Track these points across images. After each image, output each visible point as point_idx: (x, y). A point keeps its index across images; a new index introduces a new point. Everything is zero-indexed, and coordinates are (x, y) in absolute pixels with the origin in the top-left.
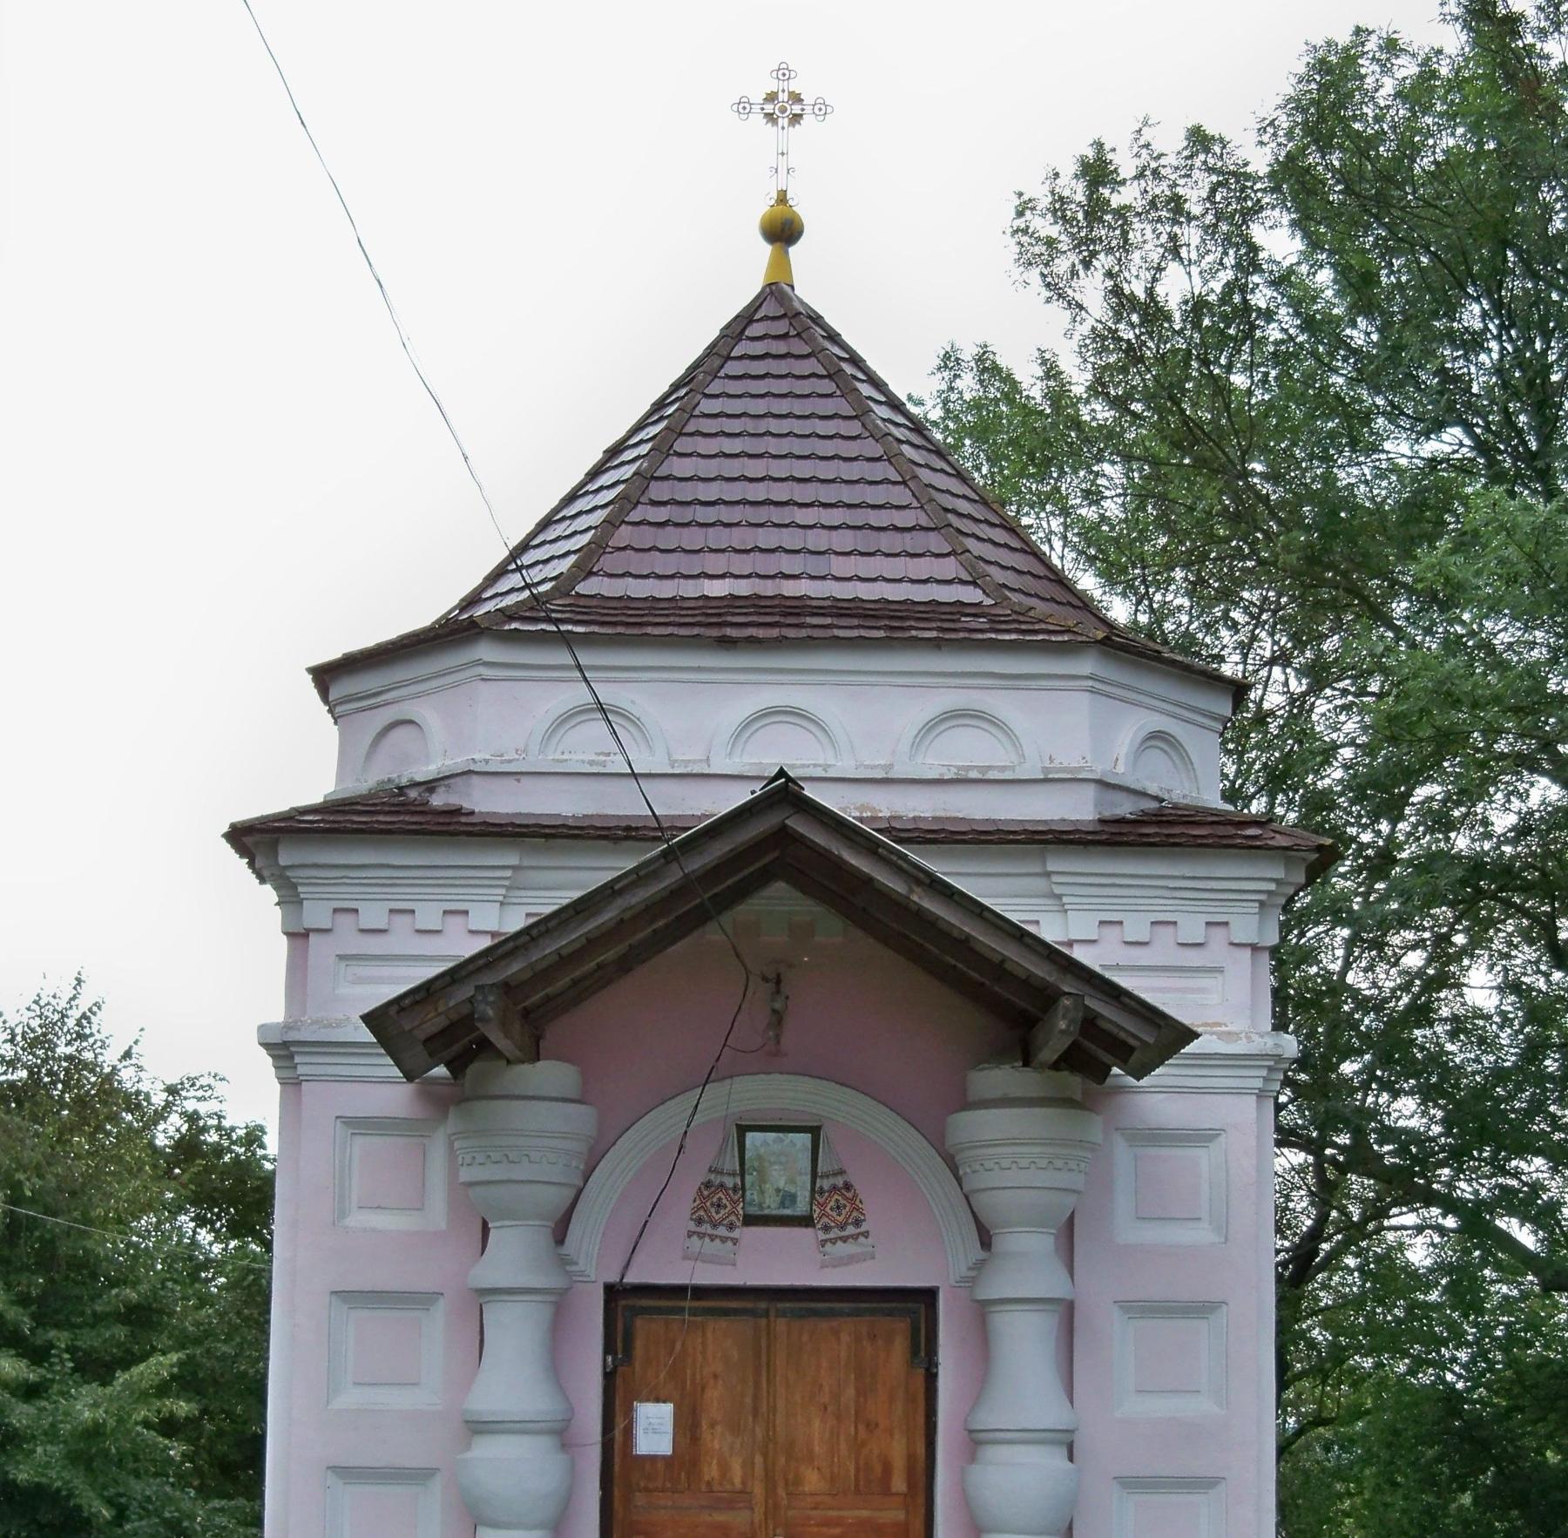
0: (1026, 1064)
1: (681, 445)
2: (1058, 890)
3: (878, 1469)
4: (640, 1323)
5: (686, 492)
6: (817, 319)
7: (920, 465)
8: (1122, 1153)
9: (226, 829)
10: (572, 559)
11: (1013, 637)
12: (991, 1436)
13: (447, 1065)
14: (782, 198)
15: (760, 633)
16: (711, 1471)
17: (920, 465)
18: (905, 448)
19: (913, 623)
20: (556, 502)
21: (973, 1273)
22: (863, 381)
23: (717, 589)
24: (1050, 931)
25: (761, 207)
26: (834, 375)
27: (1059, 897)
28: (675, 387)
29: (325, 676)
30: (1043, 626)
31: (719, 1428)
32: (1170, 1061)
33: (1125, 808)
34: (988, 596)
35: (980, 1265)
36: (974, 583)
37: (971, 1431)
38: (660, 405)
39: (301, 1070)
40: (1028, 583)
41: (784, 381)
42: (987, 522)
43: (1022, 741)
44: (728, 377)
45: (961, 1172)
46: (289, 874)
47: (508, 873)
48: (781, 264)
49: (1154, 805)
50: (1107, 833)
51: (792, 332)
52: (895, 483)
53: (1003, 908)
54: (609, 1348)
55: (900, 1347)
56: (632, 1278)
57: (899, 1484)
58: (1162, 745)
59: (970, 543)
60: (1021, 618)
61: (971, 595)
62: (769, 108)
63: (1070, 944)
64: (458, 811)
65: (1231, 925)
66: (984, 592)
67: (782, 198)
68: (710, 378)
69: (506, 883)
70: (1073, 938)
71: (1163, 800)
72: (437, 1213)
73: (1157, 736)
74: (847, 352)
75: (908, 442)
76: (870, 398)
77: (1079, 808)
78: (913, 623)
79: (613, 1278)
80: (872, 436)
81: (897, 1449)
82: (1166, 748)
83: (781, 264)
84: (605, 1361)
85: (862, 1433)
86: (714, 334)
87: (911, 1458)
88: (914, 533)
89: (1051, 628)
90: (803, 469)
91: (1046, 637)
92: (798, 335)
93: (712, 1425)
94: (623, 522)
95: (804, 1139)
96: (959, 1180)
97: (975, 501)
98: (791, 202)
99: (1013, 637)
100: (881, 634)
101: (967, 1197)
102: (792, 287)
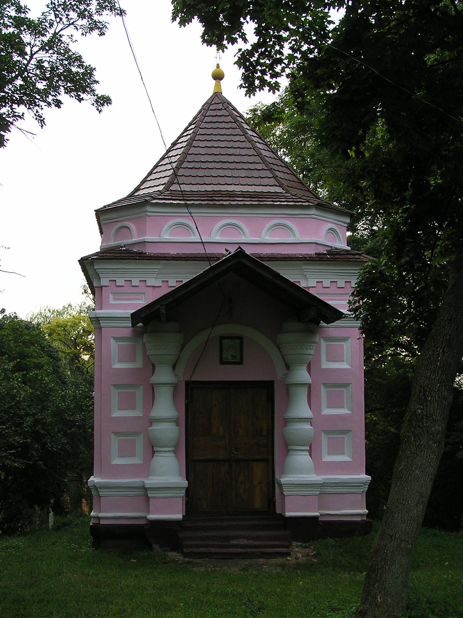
0: (299, 321)
1: (195, 144)
2: (305, 273)
5: (197, 158)
6: (230, 104)
7: (262, 149)
8: (323, 345)
9: (80, 259)
10: (167, 179)
11: (292, 203)
12: (291, 420)
13: (142, 323)
15: (225, 203)
17: (262, 149)
18: (263, 152)
19: (265, 199)
20: (159, 159)
21: (285, 377)
22: (244, 123)
23: (209, 188)
24: (303, 285)
25: (212, 68)
26: (236, 121)
27: (306, 275)
28: (190, 124)
29: (99, 213)
30: (300, 200)
32: (337, 322)
33: (323, 250)
34: (284, 190)
35: (286, 374)
36: (280, 186)
37: (284, 419)
38: (186, 130)
39: (101, 324)
40: (295, 185)
41: (215, 118)
42: (281, 166)
43: (295, 232)
44: (206, 122)
45: (281, 350)
46: (97, 271)
48: (218, 86)
49: (330, 248)
50: (319, 258)
51: (223, 108)
52: (256, 156)
53: (326, 298)
54: (186, 398)
58: (331, 231)
59: (277, 173)
60: (294, 197)
61: (279, 190)
63: (308, 288)
64: (142, 253)
65: (352, 282)
66: (283, 189)
68: (201, 123)
69: (157, 273)
70: (309, 286)
71: (332, 247)
72: (138, 364)
73: (331, 229)
74: (239, 114)
75: (258, 142)
76: (247, 129)
77: (311, 251)
78: (265, 199)
80: (248, 141)
82: (334, 233)
83: (218, 86)
84: (185, 402)
86: (200, 108)
88: (262, 171)
89: (302, 200)
90: (231, 151)
91: (301, 203)
92: (225, 109)
94: (181, 167)
95: (225, 341)
96: (280, 352)
97: (270, 151)
98: (220, 67)
99: (292, 203)
100: (257, 203)
101: (283, 357)
102: (222, 93)
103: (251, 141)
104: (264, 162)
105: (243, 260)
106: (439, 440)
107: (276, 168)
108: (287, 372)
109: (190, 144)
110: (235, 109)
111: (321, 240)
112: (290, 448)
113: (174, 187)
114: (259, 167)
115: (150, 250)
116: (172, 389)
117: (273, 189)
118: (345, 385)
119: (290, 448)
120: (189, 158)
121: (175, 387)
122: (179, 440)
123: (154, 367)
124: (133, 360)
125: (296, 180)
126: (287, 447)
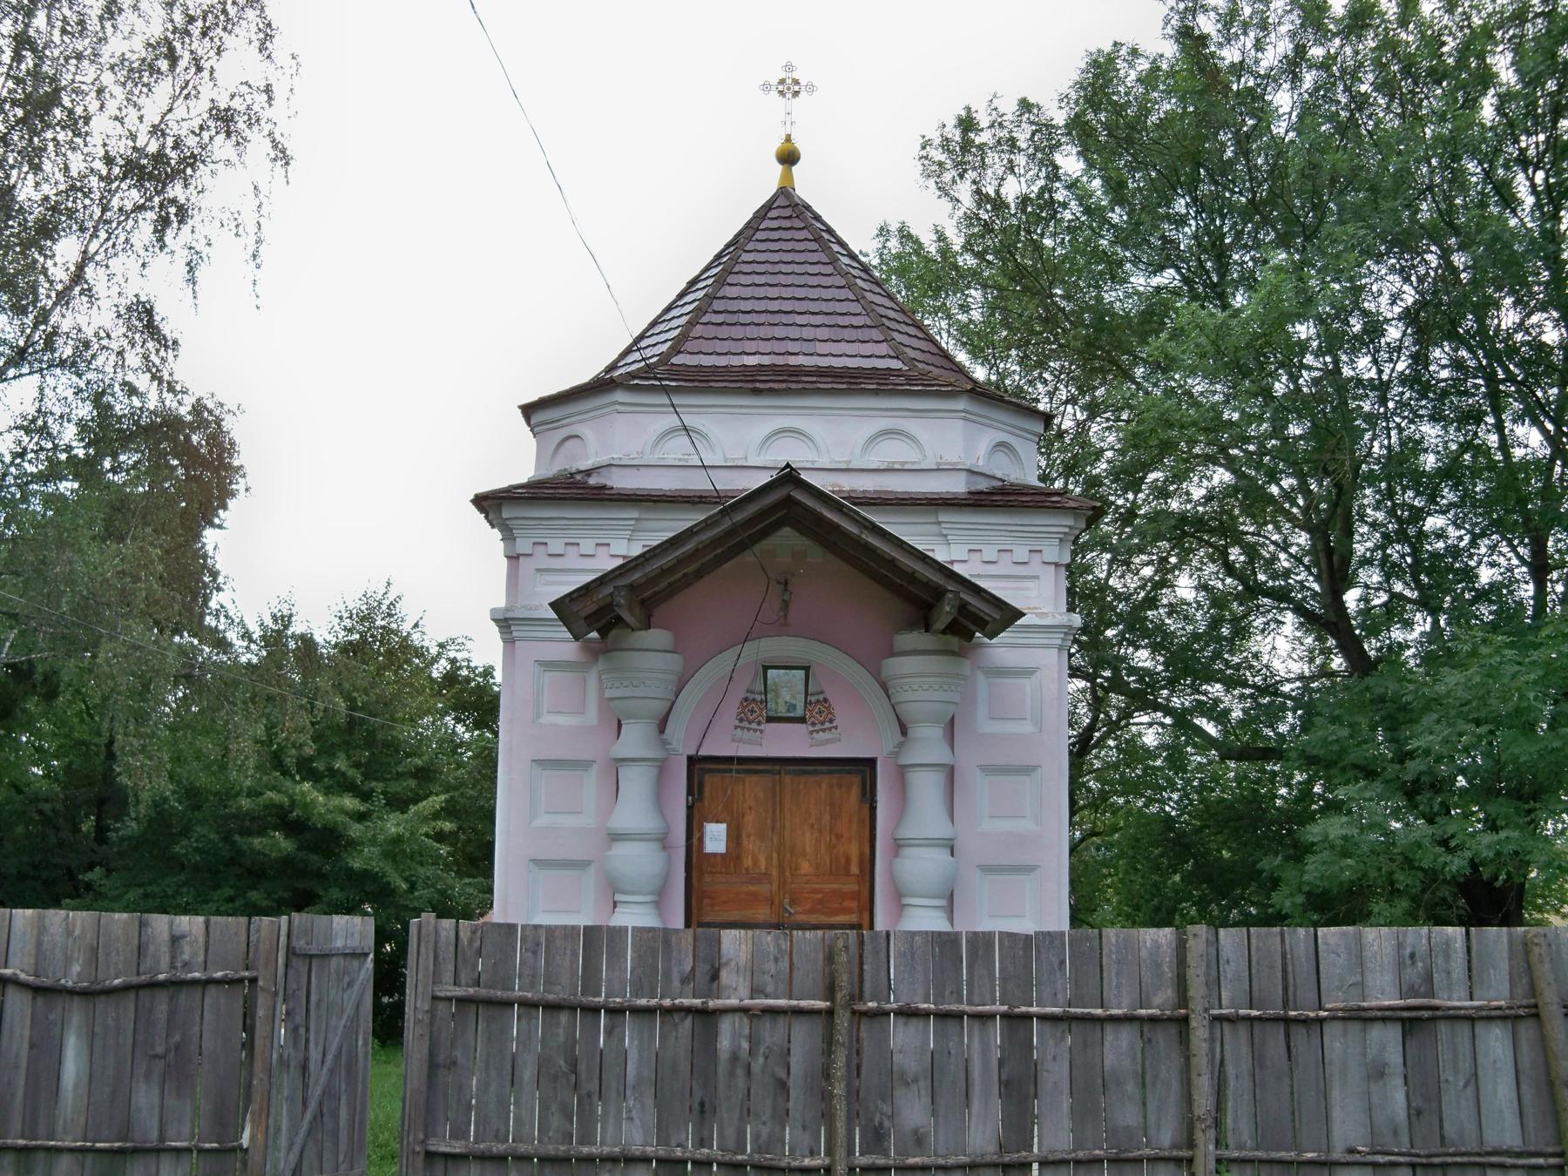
2: (945, 532)
3: (843, 861)
4: (707, 778)
5: (733, 306)
6: (808, 208)
8: (982, 681)
14: (788, 139)
15: (776, 386)
16: (748, 862)
18: (870, 296)
24: (941, 556)
25: (776, 144)
26: (826, 249)
27: (946, 536)
29: (529, 410)
31: (752, 838)
33: (983, 485)
36: (897, 358)
39: (515, 634)
47: (632, 522)
48: (787, 176)
54: (690, 792)
55: (855, 792)
56: (703, 752)
57: (855, 869)
62: (781, 88)
63: (952, 562)
67: (788, 139)
73: (1001, 445)
77: (956, 485)
79: (692, 752)
81: (854, 851)
83: (787, 176)
85: (834, 841)
87: (861, 855)
93: (749, 836)
96: (889, 697)
100: (845, 386)
103: (845, 275)
104: (869, 308)
105: (798, 495)
106: (630, 1119)
107: (891, 314)
108: (902, 739)
109: (720, 281)
110: (817, 218)
111: (981, 464)
112: (907, 901)
113: (678, 360)
114: (814, 257)
115: (621, 481)
116: (654, 772)
117: (882, 364)
118: (1027, 770)
119: (907, 901)
120: (718, 305)
121: (662, 768)
122: (666, 879)
123: (620, 725)
124: (581, 712)
125: (935, 350)
126: (900, 900)
